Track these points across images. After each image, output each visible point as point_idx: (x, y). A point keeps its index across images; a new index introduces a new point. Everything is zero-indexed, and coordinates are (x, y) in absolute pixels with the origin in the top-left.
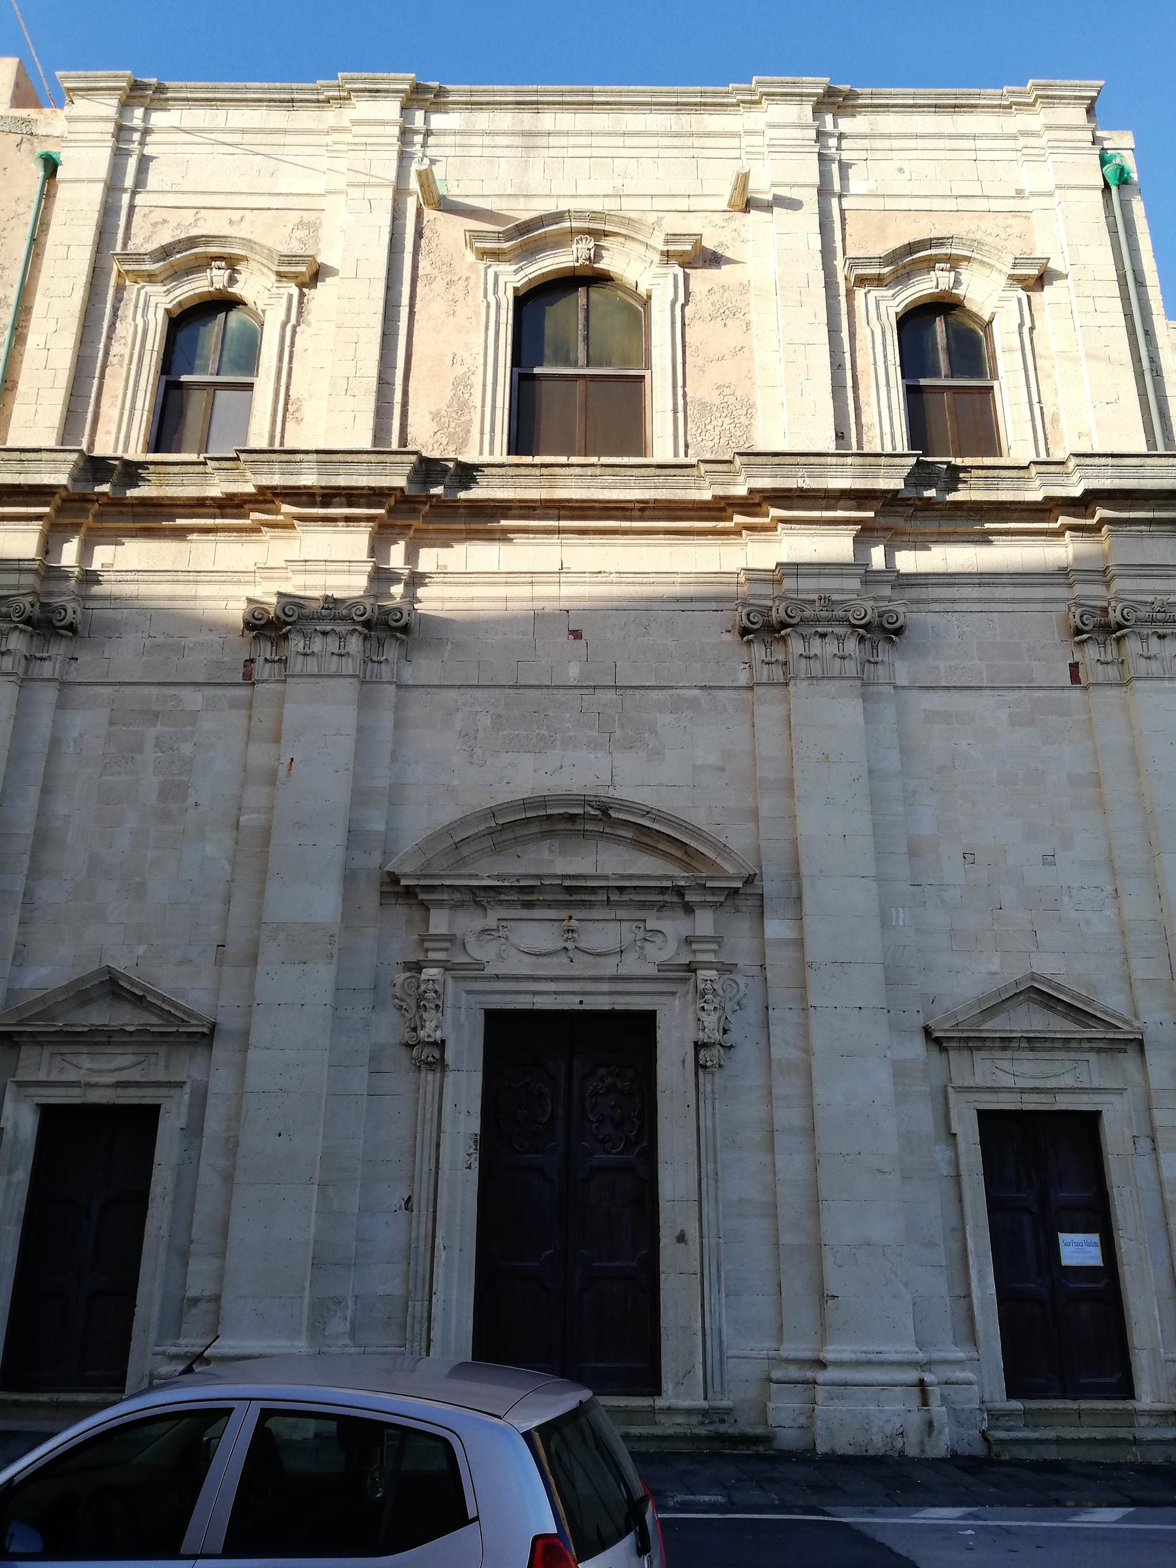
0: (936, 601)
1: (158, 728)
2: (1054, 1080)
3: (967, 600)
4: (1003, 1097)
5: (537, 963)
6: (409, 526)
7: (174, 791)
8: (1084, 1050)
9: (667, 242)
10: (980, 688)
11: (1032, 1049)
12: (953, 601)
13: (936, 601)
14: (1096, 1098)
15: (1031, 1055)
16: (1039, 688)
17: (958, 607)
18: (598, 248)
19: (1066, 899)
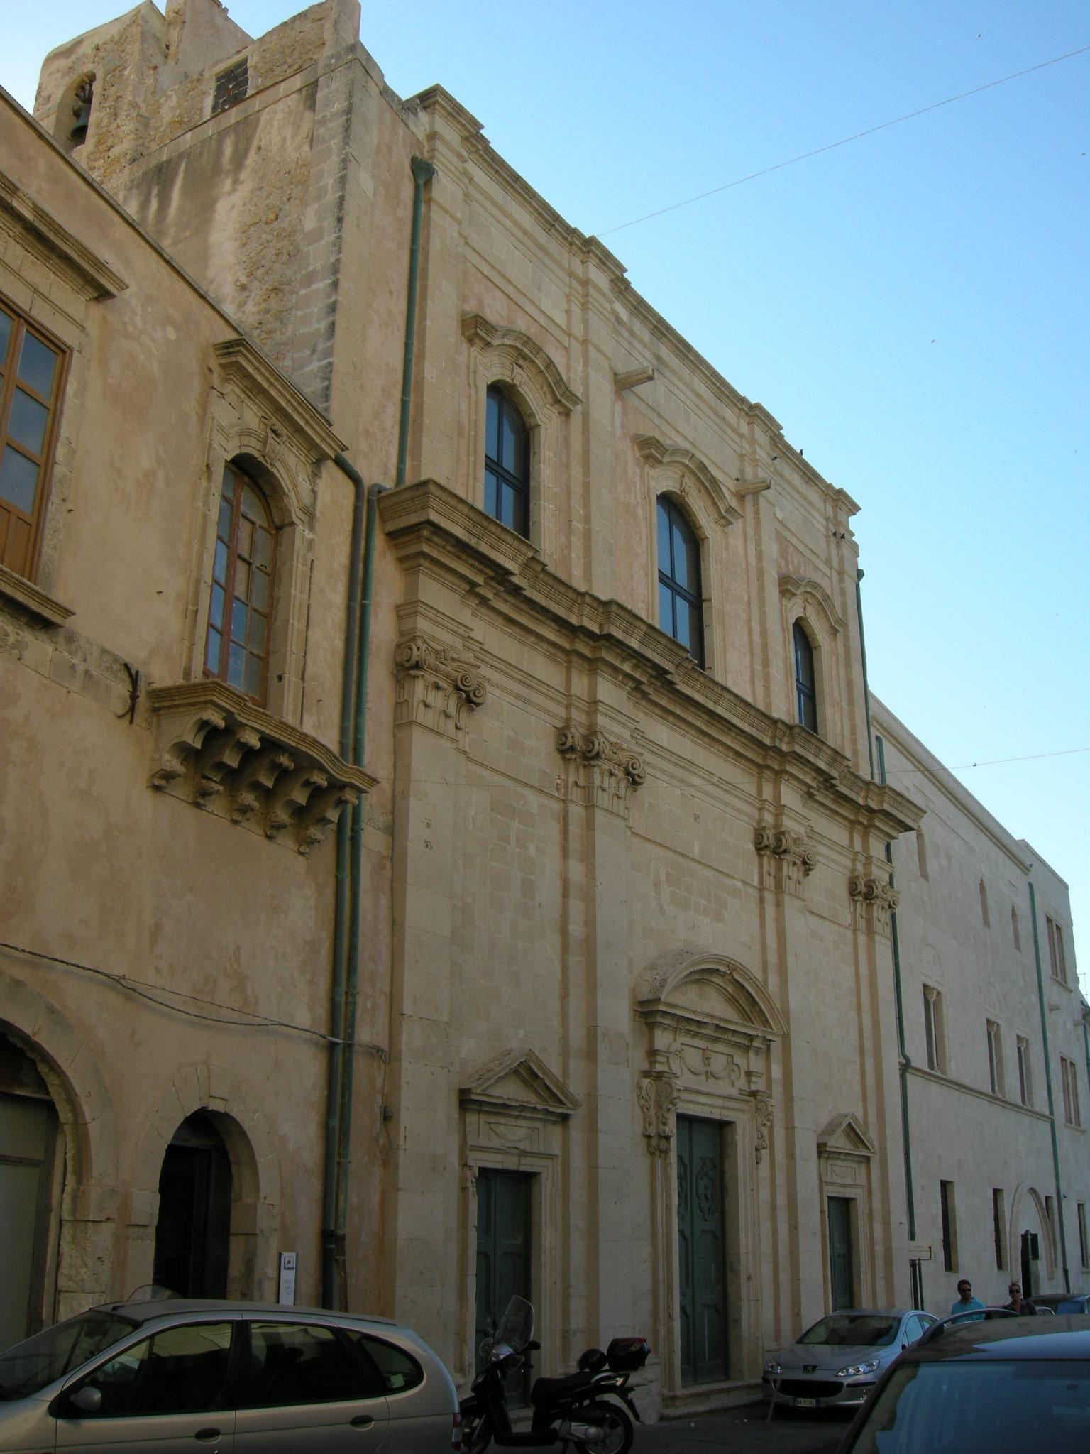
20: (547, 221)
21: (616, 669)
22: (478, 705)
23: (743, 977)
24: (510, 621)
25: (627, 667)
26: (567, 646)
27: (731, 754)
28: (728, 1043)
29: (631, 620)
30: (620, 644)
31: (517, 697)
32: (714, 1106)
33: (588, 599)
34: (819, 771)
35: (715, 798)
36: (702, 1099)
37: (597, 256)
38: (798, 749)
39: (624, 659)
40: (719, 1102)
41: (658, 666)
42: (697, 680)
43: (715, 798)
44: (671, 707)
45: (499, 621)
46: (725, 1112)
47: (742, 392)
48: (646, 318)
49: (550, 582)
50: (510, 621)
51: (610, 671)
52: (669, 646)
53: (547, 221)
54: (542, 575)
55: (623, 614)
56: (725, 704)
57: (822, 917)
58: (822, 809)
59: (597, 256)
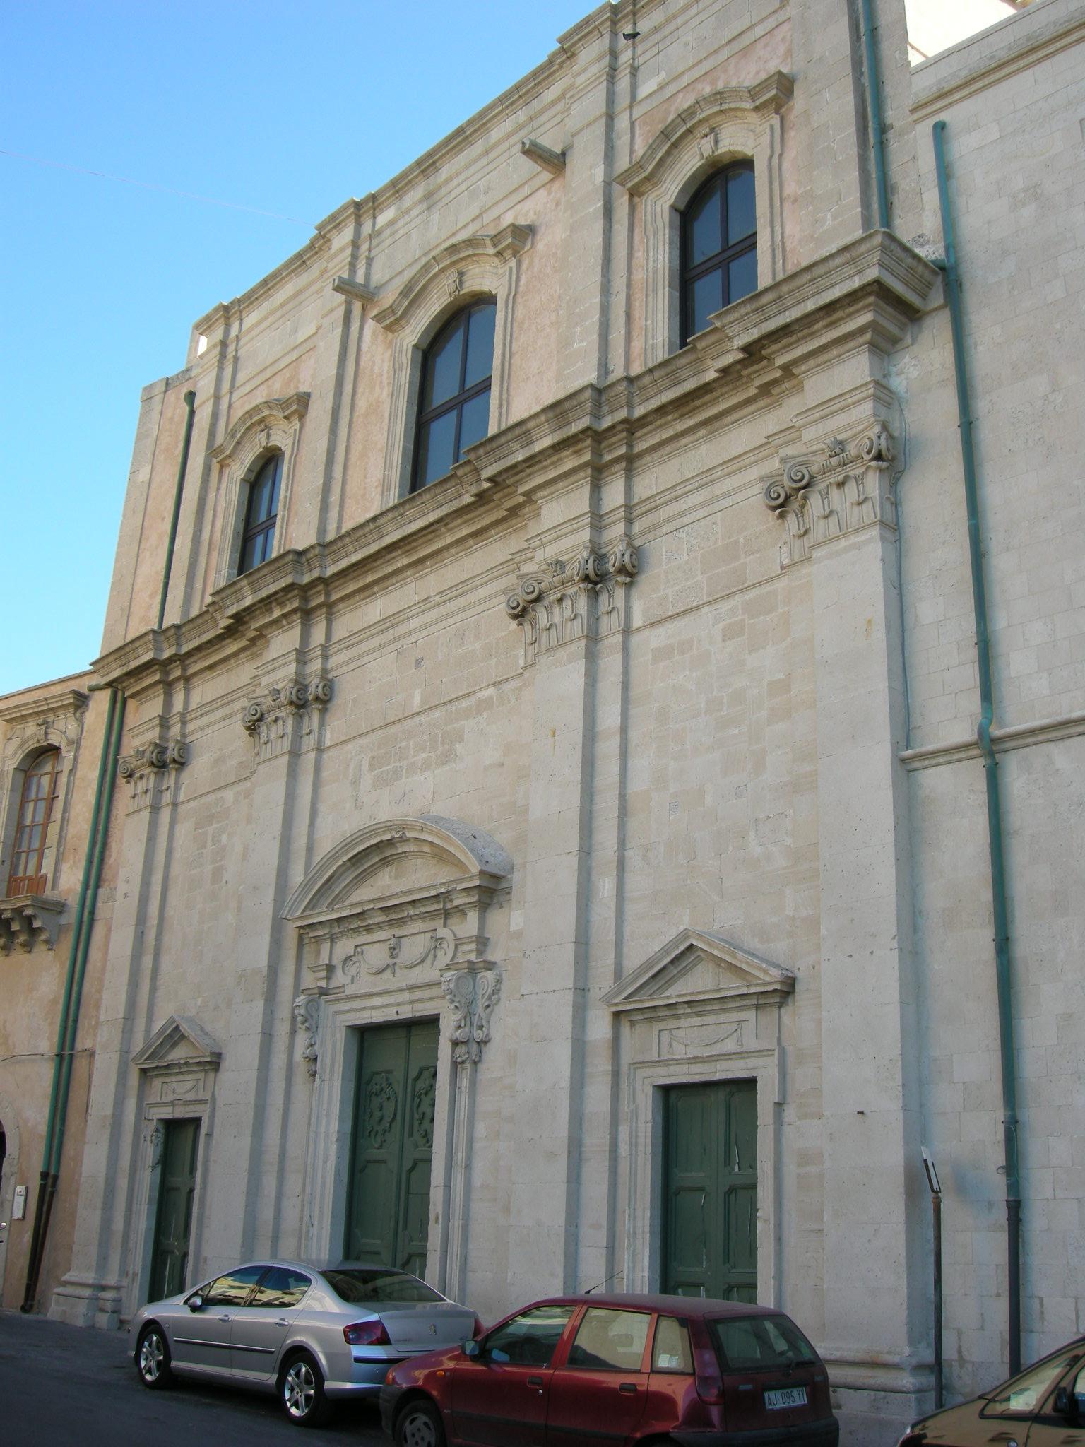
0: (667, 521)
1: (214, 826)
2: (719, 1045)
3: (693, 509)
4: (674, 1069)
5: (693, 1051)
6: (847, 478)
7: (217, 874)
8: (738, 1009)
9: (495, 245)
10: (698, 607)
11: (698, 1014)
12: (682, 514)
13: (667, 521)
14: (751, 1063)
15: (697, 1021)
16: (752, 586)
17: (687, 520)
18: (461, 274)
19: (752, 834)
20: (300, 266)
21: (275, 622)
22: (782, 516)
23: (347, 852)
24: (211, 667)
25: (277, 613)
26: (244, 643)
27: (471, 542)
28: (420, 917)
29: (233, 590)
30: (532, 461)
31: (224, 719)
32: (398, 1004)
33: (211, 610)
34: (557, 447)
35: (445, 618)
36: (377, 1001)
37: (330, 230)
38: (234, 609)
39: (270, 611)
40: (406, 996)
41: (862, 288)
42: (344, 546)
43: (445, 618)
44: (361, 584)
45: (208, 675)
46: (419, 1006)
47: (543, 58)
48: (410, 182)
49: (191, 626)
50: (211, 667)
51: (274, 627)
52: (272, 568)
53: (300, 266)
54: (327, 552)
55: (223, 595)
56: (391, 526)
57: (687, 612)
58: (684, 441)
59: (330, 230)
